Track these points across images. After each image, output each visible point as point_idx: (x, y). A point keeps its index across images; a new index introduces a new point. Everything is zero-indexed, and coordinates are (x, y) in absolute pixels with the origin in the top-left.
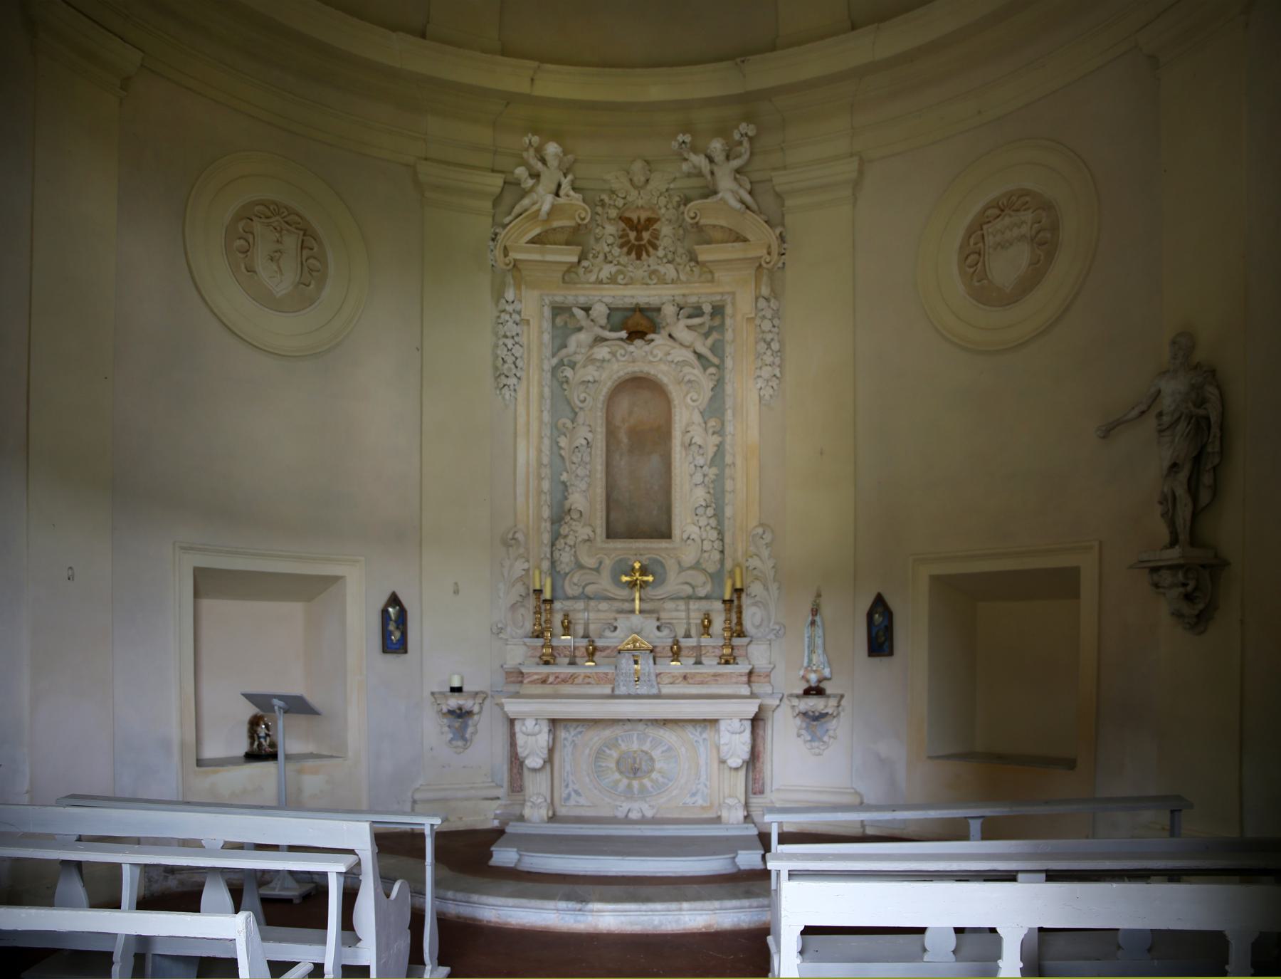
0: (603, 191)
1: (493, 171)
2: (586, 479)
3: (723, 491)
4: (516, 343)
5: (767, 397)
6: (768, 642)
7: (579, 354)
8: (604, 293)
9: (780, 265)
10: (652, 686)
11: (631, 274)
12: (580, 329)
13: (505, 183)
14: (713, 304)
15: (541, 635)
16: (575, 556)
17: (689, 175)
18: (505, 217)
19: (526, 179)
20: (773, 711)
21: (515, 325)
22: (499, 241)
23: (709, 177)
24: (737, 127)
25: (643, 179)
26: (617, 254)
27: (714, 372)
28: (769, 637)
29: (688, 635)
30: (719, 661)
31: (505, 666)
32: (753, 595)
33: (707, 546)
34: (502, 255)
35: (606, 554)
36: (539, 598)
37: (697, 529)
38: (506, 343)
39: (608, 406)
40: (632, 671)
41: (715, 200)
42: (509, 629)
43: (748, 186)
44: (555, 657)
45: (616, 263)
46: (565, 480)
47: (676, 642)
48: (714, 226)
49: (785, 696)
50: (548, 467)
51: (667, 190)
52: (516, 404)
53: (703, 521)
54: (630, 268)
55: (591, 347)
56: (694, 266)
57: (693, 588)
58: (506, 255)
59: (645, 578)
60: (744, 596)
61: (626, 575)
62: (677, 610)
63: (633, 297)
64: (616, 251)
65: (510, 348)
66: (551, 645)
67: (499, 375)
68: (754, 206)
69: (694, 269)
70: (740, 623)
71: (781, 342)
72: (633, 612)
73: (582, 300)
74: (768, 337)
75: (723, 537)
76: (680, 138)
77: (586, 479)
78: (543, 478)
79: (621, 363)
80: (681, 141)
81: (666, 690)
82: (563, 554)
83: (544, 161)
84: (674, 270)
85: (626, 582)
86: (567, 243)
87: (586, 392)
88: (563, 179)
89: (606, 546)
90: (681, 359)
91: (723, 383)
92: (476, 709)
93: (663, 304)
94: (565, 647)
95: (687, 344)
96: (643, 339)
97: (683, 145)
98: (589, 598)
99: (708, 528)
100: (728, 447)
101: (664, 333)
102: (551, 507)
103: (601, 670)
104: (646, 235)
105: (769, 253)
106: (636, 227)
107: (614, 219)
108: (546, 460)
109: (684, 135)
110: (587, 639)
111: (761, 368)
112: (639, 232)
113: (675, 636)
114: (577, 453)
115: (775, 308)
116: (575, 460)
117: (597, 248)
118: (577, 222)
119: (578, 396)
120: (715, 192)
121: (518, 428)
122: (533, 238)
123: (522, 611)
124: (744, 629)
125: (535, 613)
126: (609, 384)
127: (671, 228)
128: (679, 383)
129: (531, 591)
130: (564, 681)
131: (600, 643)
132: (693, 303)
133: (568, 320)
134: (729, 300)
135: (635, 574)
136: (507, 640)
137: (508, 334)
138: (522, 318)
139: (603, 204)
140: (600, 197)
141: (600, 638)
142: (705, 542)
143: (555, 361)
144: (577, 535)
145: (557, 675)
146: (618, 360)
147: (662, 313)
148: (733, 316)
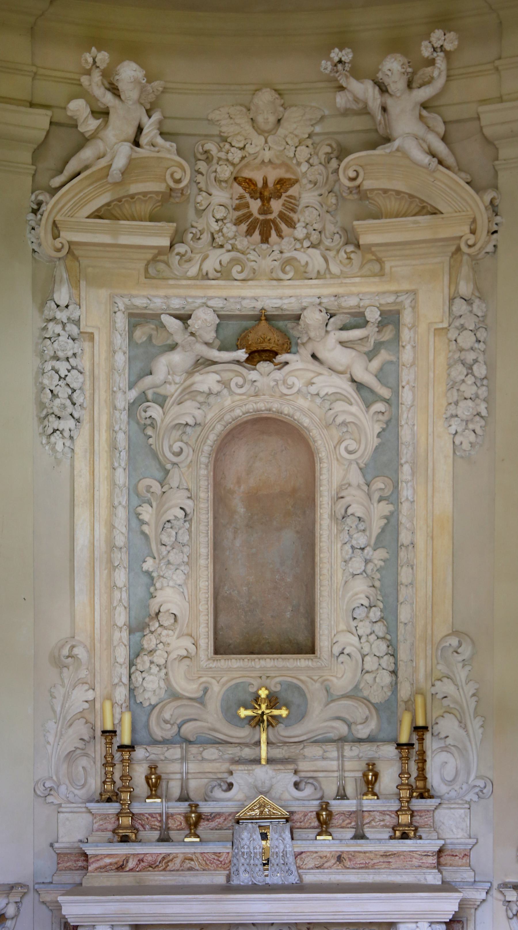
0: (207, 136)
1: (32, 105)
2: (182, 568)
3: (397, 585)
4: (73, 368)
5: (466, 446)
6: (467, 806)
7: (170, 384)
8: (211, 293)
9: (490, 248)
10: (289, 872)
11: (253, 263)
12: (173, 347)
13: (51, 123)
14: (382, 308)
15: (114, 798)
16: (167, 680)
17: (346, 113)
18: (53, 177)
19: (87, 117)
20: (476, 909)
21: (70, 341)
22: (46, 215)
23: (379, 116)
24: (427, 36)
25: (272, 119)
26: (231, 235)
27: (383, 410)
28: (467, 798)
29: (342, 796)
30: (392, 834)
31: (56, 845)
32: (442, 735)
33: (370, 663)
34: (50, 236)
35: (213, 678)
36: (112, 743)
37: (354, 640)
38: (57, 368)
39: (216, 460)
40: (259, 850)
41: (388, 151)
42: (63, 789)
43: (441, 129)
44: (138, 830)
45: (230, 247)
46: (151, 570)
47: (325, 806)
48: (385, 191)
49: (495, 885)
50: (124, 550)
51: (310, 136)
52: (72, 458)
53: (364, 628)
54: (253, 256)
55: (190, 373)
56: (352, 252)
57: (349, 726)
58: (56, 236)
59: (276, 712)
60: (428, 736)
61: (246, 708)
62: (324, 758)
63: (256, 299)
64: (230, 229)
65: (63, 376)
66: (131, 812)
67: (47, 415)
68: (450, 160)
69: (352, 256)
70: (422, 776)
71: (490, 366)
72: (257, 761)
73: (176, 304)
74: (470, 357)
75: (395, 650)
76: (335, 55)
77: (182, 568)
78: (115, 568)
79: (237, 398)
80: (336, 59)
81: (309, 878)
82: (149, 678)
83: (114, 90)
84: (322, 260)
85: (247, 717)
86: (152, 218)
87: (182, 441)
88: (145, 118)
89: (213, 665)
90: (331, 390)
91: (398, 425)
92: (11, 911)
93: (304, 309)
94: (151, 815)
95: (340, 368)
96: (271, 361)
97: (340, 66)
98: (189, 742)
99: (373, 637)
100: (403, 519)
101: (305, 352)
102: (129, 609)
103: (210, 848)
104: (276, 205)
105: (473, 232)
106: (261, 193)
107: (226, 182)
108: (120, 540)
109: (341, 50)
110: (187, 803)
111: (456, 403)
112: (265, 200)
113: (321, 798)
114: (170, 530)
115: (480, 314)
116: (165, 539)
117: (200, 224)
118: (168, 185)
119: (170, 447)
120: (388, 140)
121: (76, 493)
122: (98, 210)
123: (84, 762)
124: (429, 786)
125: (105, 765)
126: (219, 428)
127: (316, 193)
128: (328, 426)
129: (98, 733)
130: (153, 866)
131: (205, 808)
132: (351, 308)
133: (154, 333)
134: (407, 303)
135: (260, 705)
136: (60, 805)
137: (60, 354)
138: (81, 330)
139: (208, 158)
140: (203, 146)
141: (206, 800)
142: (367, 659)
143: (133, 394)
144: (168, 649)
145: (141, 857)
146: (232, 393)
147: (301, 322)
148: (414, 327)
